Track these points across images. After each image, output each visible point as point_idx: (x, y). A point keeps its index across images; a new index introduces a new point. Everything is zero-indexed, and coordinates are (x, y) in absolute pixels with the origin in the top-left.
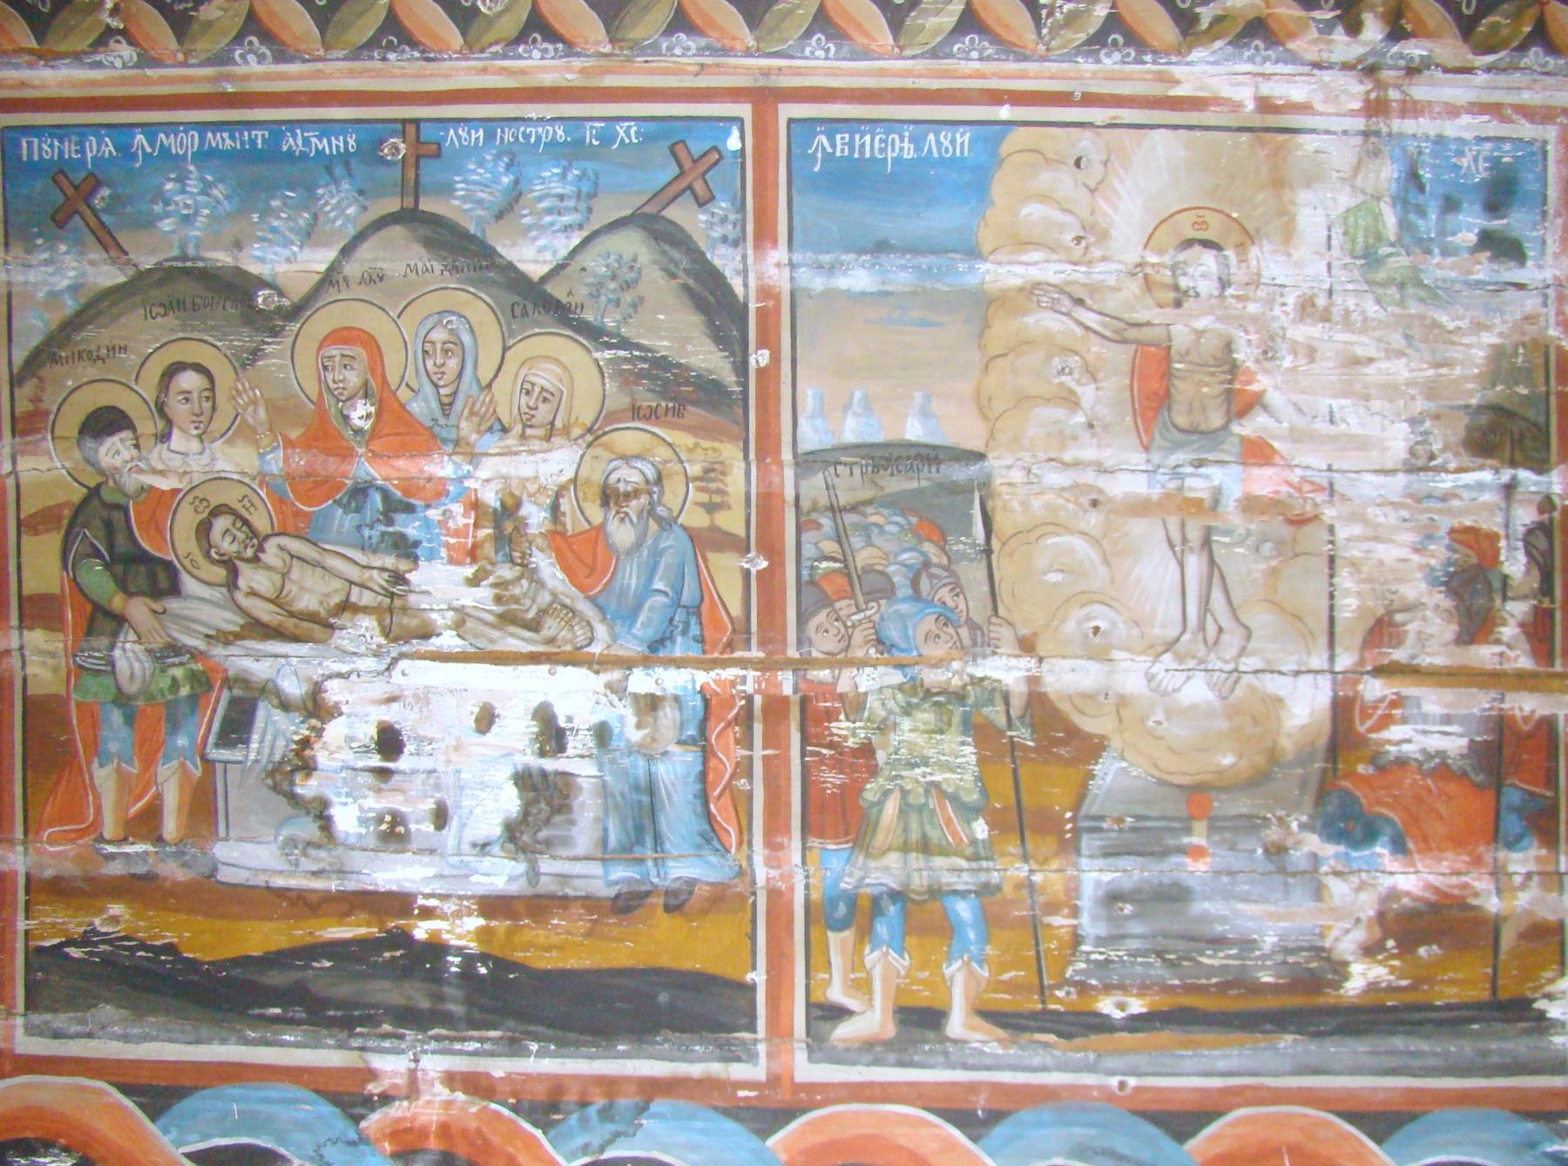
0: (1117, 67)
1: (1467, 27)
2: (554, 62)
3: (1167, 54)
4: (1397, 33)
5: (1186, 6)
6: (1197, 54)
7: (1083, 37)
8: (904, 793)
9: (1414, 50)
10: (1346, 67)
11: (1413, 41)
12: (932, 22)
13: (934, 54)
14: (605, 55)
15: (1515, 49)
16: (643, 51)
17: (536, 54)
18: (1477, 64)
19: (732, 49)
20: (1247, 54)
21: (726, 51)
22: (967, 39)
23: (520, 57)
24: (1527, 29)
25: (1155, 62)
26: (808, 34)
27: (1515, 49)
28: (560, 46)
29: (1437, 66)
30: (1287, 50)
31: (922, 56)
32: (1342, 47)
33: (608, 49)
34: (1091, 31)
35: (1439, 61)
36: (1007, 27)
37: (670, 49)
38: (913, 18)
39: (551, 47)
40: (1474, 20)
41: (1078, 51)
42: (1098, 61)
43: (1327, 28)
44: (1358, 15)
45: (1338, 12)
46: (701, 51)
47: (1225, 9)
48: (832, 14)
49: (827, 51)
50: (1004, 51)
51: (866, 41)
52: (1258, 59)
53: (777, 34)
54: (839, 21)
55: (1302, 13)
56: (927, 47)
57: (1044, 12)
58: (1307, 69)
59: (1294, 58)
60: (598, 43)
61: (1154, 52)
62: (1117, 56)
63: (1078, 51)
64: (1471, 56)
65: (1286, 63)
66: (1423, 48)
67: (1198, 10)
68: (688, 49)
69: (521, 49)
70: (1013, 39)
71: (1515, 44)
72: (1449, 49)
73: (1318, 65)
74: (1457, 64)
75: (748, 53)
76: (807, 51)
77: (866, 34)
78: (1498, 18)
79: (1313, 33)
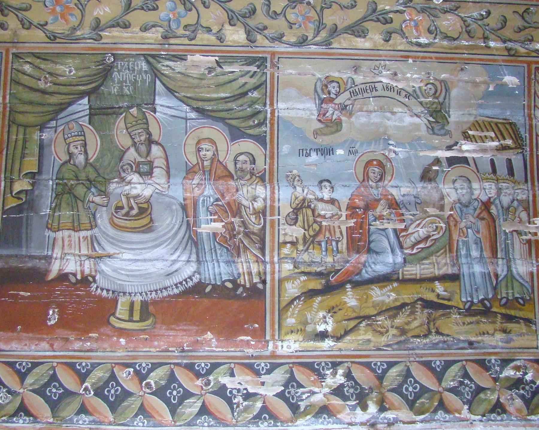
0: (266, 428)
1: (411, 404)
2: (28, 425)
3: (287, 422)
4: (382, 409)
5: (294, 402)
6: (300, 421)
7: (251, 416)
8: (406, 229)
9: (390, 415)
10: (362, 424)
11: (389, 412)
12: (188, 410)
13: (189, 424)
14: (50, 423)
15: (432, 412)
16: (66, 422)
17: (21, 421)
18: (417, 419)
19: (104, 422)
20: (321, 420)
21: (101, 423)
22: (203, 418)
23: (14, 422)
24: (436, 404)
25: (282, 426)
26: (136, 415)
27: (432, 412)
28: (31, 418)
29: (400, 421)
30: (337, 418)
31: (184, 425)
32: (360, 416)
33: (51, 420)
34: (255, 414)
35: (401, 419)
36: (219, 412)
37: (77, 421)
38: (180, 410)
39: (27, 419)
40: (414, 402)
41: (249, 422)
42: (258, 426)
43: (353, 408)
44: (366, 402)
45: (358, 401)
46: (91, 422)
47: (310, 402)
48: (146, 407)
49: (144, 423)
50: (218, 423)
51: (160, 419)
52: (325, 423)
53: (123, 415)
54: (150, 411)
55: (343, 403)
56: (186, 421)
57: (235, 406)
58: (346, 426)
59: (341, 422)
60: (47, 418)
61: (282, 422)
62: (266, 424)
63: (249, 422)
64: (414, 416)
65: (337, 424)
66: (394, 414)
67: (299, 403)
68: (85, 421)
69: (15, 419)
70: (221, 417)
71: (432, 410)
72: (405, 414)
73: (351, 424)
74: (409, 420)
75: (110, 424)
76: (135, 423)
77: (161, 416)
78: (423, 400)
79: (348, 410)
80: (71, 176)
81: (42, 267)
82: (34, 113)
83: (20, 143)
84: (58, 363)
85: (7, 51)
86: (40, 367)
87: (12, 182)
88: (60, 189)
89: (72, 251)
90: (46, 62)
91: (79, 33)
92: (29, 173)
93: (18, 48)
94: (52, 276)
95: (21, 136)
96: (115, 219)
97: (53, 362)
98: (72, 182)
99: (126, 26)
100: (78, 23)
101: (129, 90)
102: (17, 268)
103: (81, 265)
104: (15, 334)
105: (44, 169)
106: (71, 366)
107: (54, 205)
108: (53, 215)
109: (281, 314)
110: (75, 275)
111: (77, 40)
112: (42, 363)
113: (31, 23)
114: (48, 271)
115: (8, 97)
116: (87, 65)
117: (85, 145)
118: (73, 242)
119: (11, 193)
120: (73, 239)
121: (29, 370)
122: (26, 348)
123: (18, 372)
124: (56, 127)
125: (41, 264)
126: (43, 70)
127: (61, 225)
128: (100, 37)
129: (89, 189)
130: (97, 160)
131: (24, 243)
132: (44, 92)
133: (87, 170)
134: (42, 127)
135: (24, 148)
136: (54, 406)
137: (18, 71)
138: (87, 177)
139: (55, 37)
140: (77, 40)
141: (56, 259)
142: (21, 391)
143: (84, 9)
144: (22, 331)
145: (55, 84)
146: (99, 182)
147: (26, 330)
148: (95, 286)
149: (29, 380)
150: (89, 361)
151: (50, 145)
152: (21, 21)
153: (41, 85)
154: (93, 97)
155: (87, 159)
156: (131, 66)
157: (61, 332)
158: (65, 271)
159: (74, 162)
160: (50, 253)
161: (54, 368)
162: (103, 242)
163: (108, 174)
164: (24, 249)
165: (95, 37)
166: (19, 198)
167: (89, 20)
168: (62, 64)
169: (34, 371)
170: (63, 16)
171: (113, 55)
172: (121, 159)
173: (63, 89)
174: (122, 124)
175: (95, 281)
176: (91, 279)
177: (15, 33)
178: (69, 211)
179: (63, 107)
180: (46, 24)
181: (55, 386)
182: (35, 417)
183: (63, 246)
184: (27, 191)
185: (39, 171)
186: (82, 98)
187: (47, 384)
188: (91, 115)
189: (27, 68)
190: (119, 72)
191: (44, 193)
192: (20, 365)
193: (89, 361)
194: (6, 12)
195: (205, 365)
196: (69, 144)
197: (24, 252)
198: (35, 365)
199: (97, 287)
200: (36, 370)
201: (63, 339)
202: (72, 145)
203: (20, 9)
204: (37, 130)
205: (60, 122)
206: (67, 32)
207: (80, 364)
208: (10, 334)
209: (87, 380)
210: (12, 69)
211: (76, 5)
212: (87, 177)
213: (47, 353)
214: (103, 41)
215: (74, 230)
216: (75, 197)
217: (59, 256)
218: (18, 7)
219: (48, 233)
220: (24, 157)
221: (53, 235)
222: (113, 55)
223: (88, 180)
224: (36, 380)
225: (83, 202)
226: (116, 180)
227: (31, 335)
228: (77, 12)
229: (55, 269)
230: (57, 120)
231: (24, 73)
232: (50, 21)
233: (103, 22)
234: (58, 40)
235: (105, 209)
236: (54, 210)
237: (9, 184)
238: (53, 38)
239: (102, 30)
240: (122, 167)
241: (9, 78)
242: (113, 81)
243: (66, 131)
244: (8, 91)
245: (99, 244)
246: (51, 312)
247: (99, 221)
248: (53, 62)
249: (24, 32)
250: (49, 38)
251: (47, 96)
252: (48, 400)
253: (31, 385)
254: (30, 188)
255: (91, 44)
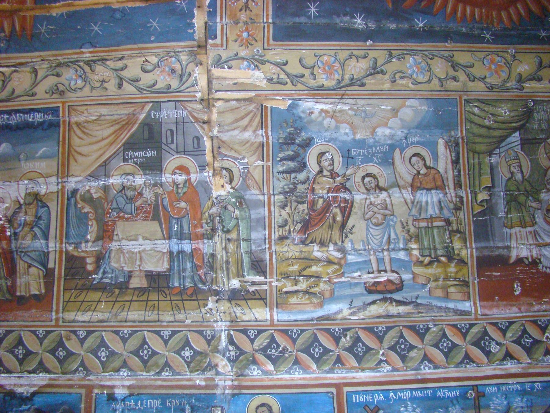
23: (505, 365)
26: (422, 362)
33: (529, 361)
60: (526, 360)
80: (515, 189)
81: (505, 254)
82: (483, 143)
83: (477, 166)
84: (526, 321)
85: (460, 98)
86: (514, 324)
87: (476, 194)
88: (509, 197)
89: (523, 242)
90: (488, 106)
91: (508, 85)
92: (486, 187)
93: (468, 96)
94: (512, 260)
95: (476, 161)
96: (547, 218)
97: (442, 324)
98: (516, 193)
99: (540, 80)
100: (507, 77)
101: (545, 126)
102: (489, 256)
103: (530, 251)
104: (495, 303)
105: (496, 185)
106: (534, 322)
107: (506, 209)
108: (507, 217)
109: (457, 287)
110: (527, 258)
111: (507, 90)
112: (516, 322)
113: (475, 77)
114: (509, 257)
115: (464, 132)
116: (516, 108)
117: (520, 166)
118: (523, 236)
119: (476, 202)
120: (522, 233)
121: (508, 328)
122: (502, 312)
123: (500, 329)
124: (500, 153)
125: (504, 252)
126: (487, 112)
127: (513, 224)
128: (522, 88)
129: (527, 197)
130: (530, 176)
131: (490, 237)
132: (489, 128)
133: (524, 183)
134: (490, 154)
135: (480, 169)
136: (529, 351)
137: (469, 112)
138: (525, 188)
139: (492, 88)
140: (507, 90)
141: (514, 248)
142: (505, 342)
143: (511, 67)
144: (499, 300)
145: (495, 122)
146: (533, 192)
147: (500, 299)
148: (541, 266)
149: (509, 334)
150: (546, 318)
151: (497, 167)
152: (468, 75)
153: (487, 123)
154: (522, 131)
155: (523, 176)
156: (545, 109)
157: (524, 299)
158: (521, 256)
159: (515, 178)
160: (509, 244)
161: (523, 325)
162: (542, 234)
163: (538, 187)
164: (492, 242)
165: (519, 87)
166: (482, 206)
167: (514, 76)
168: (499, 108)
169: (511, 327)
170: (496, 72)
171: (533, 100)
172: (545, 176)
173: (503, 126)
174: (543, 150)
175: (541, 262)
176: (538, 261)
177: (465, 84)
178: (517, 214)
179: (503, 139)
180: (485, 77)
181: (526, 337)
182: (518, 360)
183: (517, 238)
184: (486, 200)
185: (492, 185)
186: (515, 132)
187: (521, 337)
188: (522, 145)
189: (476, 110)
190: (538, 112)
191: (499, 202)
192: (501, 324)
193: (546, 318)
194: (456, 68)
195: (339, 330)
196: (510, 166)
197: (491, 244)
198: (511, 323)
199: (543, 267)
200: (513, 327)
201: (528, 304)
202: (512, 166)
203: (465, 67)
204: (487, 156)
205: (502, 150)
206: (500, 84)
207: (540, 321)
208: (491, 303)
209: (547, 331)
210: (465, 111)
211: (505, 63)
212: (525, 188)
213: (518, 315)
214: (525, 90)
215: (522, 227)
216: (519, 203)
217: (515, 245)
218: (464, 65)
219: (505, 230)
220: (481, 176)
221: (509, 231)
222: (533, 100)
223: (526, 191)
224: (513, 334)
225: (525, 207)
226: (544, 190)
227: (505, 303)
228: (506, 69)
229: (514, 255)
230: (500, 148)
231: (474, 114)
232: (488, 76)
233: (524, 77)
234: (494, 90)
235: (539, 211)
236: (507, 213)
237: (473, 195)
238: (491, 88)
239: (524, 82)
240: (547, 181)
241: (464, 117)
242: (534, 119)
243: (507, 155)
244: (464, 127)
245: (540, 236)
246: (515, 286)
247: (537, 220)
248: (493, 106)
249: (471, 84)
250: (489, 88)
251: (491, 131)
252: (523, 347)
253: (511, 337)
254: (488, 198)
255: (516, 92)
